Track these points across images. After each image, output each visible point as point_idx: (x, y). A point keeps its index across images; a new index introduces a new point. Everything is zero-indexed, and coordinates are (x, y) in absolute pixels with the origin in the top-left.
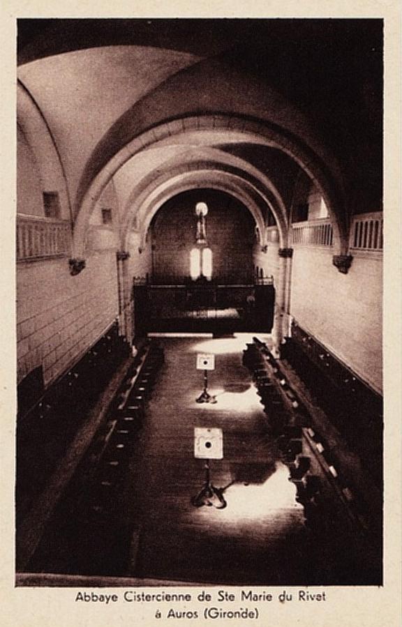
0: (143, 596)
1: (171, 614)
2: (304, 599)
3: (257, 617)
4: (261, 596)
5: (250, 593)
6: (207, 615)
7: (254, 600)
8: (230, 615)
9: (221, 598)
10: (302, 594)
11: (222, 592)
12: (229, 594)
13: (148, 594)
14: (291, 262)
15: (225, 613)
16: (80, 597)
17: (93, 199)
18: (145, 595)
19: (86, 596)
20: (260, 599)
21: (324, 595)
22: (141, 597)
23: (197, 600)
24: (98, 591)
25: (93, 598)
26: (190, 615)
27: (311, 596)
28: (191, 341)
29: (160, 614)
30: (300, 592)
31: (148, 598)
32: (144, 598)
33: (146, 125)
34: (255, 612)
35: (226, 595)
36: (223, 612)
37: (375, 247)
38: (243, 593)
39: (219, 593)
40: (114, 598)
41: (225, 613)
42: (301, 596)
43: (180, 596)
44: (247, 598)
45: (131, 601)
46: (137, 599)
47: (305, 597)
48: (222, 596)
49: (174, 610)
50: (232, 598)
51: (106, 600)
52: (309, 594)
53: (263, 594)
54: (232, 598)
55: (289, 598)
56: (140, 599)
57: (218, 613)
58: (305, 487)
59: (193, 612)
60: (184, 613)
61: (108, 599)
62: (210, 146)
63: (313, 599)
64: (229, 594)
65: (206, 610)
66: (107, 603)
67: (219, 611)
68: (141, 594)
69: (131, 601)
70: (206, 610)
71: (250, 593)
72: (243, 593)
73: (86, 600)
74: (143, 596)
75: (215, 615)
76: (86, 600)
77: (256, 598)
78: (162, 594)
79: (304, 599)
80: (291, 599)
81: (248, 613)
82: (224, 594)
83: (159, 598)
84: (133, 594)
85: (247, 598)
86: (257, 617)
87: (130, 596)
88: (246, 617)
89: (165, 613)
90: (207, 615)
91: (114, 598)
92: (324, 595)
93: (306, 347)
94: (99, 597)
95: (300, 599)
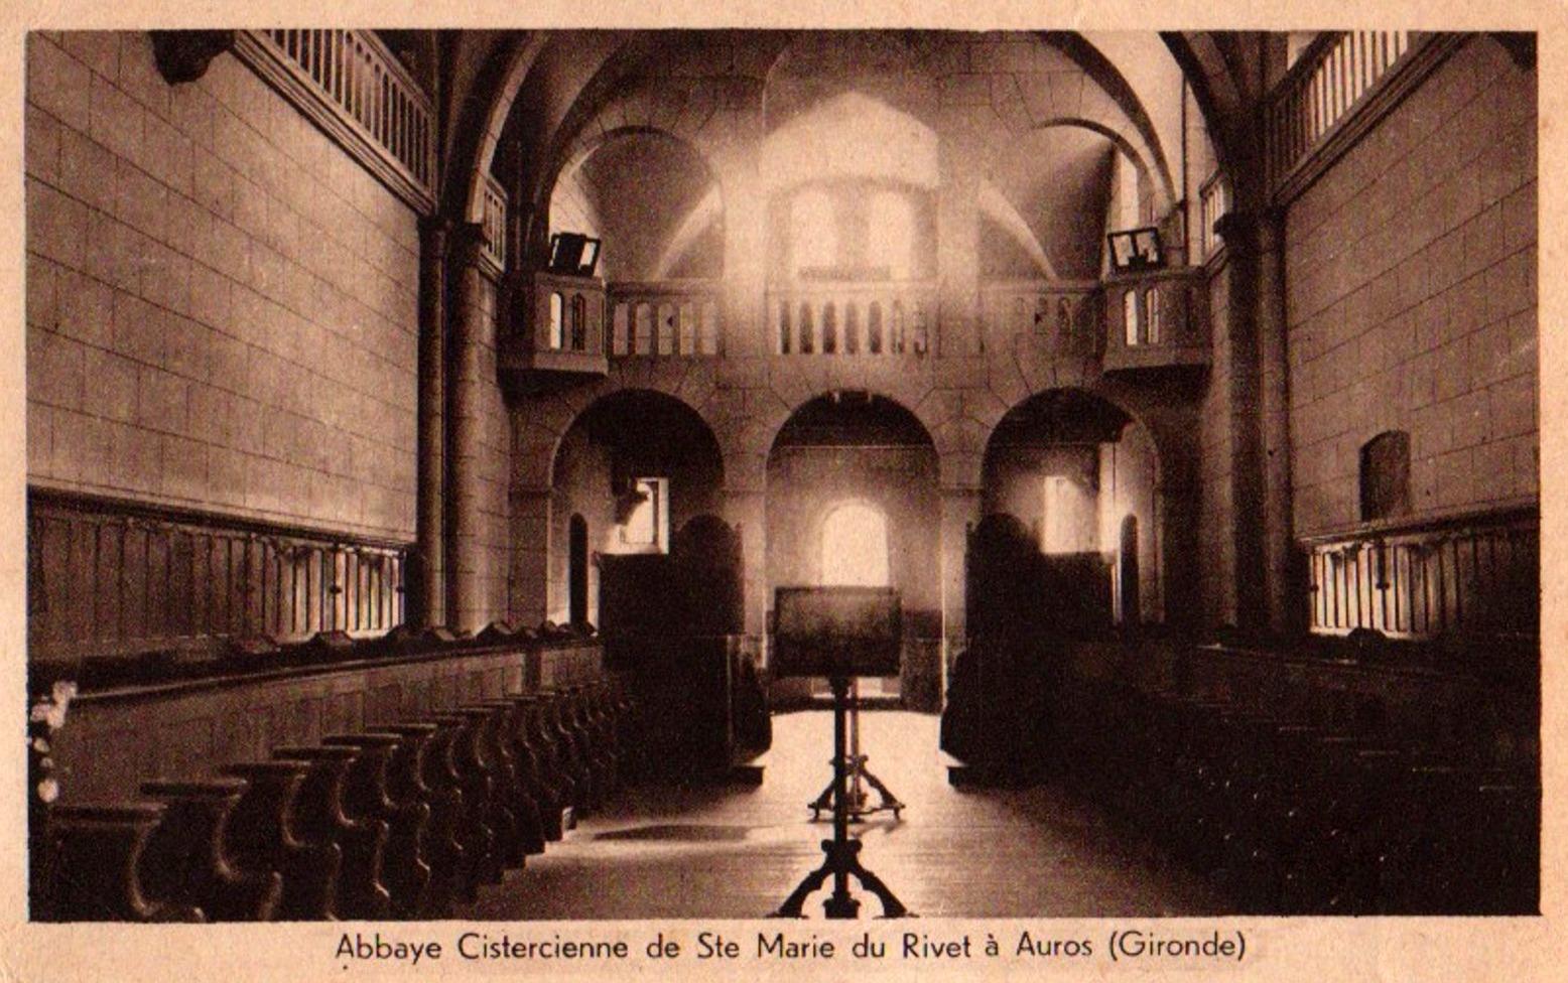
0: (506, 944)
2: (916, 955)
3: (1240, 958)
5: (780, 938)
6: (1117, 949)
7: (788, 955)
9: (705, 951)
12: (725, 942)
15: (1160, 944)
16: (345, 946)
18: (512, 943)
19: (360, 946)
20: (804, 954)
22: (501, 948)
25: (378, 949)
26: (1072, 948)
27: (933, 946)
28: (581, 384)
35: (719, 944)
36: (1156, 940)
37: (1384, 36)
38: (761, 938)
40: (433, 950)
42: (907, 947)
43: (582, 946)
44: (770, 950)
46: (490, 952)
49: (1031, 936)
51: (411, 955)
52: (929, 941)
55: (878, 951)
56: (499, 953)
57: (1143, 944)
58: (748, 764)
59: (1080, 943)
61: (418, 954)
63: (938, 954)
64: (725, 942)
65: (1115, 934)
67: (1146, 939)
68: (502, 941)
71: (780, 938)
72: (761, 938)
74: (506, 944)
76: (360, 955)
78: (554, 942)
79: (916, 955)
80: (882, 954)
81: (1220, 943)
82: (711, 941)
84: (481, 941)
85: (770, 950)
86: (1240, 958)
87: (471, 946)
90: (1117, 949)
91: (433, 950)
92: (967, 944)
94: (394, 947)
95: (906, 955)
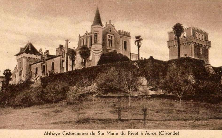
0: (70, 133)
1: (147, 133)
4: (114, 133)
5: (110, 132)
6: (160, 133)
8: (169, 134)
9: (99, 134)
10: (129, 132)
11: (99, 132)
12: (102, 133)
13: (71, 132)
14: (130, 40)
15: (166, 133)
17: (145, 46)
19: (48, 133)
21: (138, 133)
22: (69, 134)
23: (120, 134)
24: (53, 131)
29: (142, 133)
30: (129, 132)
31: (71, 134)
32: (70, 134)
33: (181, 47)
34: (178, 133)
35: (101, 133)
38: (107, 132)
39: (98, 132)
41: (166, 133)
42: (129, 133)
44: (109, 134)
45: (65, 135)
46: (67, 134)
47: (130, 134)
48: (99, 133)
50: (103, 134)
51: (56, 135)
53: (115, 133)
54: (103, 134)
57: (164, 133)
60: (151, 133)
61: (56, 135)
62: (98, 8)
63: (133, 134)
64: (102, 133)
66: (56, 136)
67: (164, 132)
69: (65, 135)
70: (160, 132)
71: (110, 132)
72: (107, 132)
73: (48, 135)
74: (70, 133)
75: (163, 134)
76: (48, 135)
77: (112, 134)
78: (77, 133)
80: (125, 134)
82: (100, 133)
83: (76, 134)
85: (109, 134)
87: (64, 133)
88: (175, 134)
89: (144, 134)
90: (160, 133)
93: (200, 80)
94: (53, 134)
95: (129, 134)
